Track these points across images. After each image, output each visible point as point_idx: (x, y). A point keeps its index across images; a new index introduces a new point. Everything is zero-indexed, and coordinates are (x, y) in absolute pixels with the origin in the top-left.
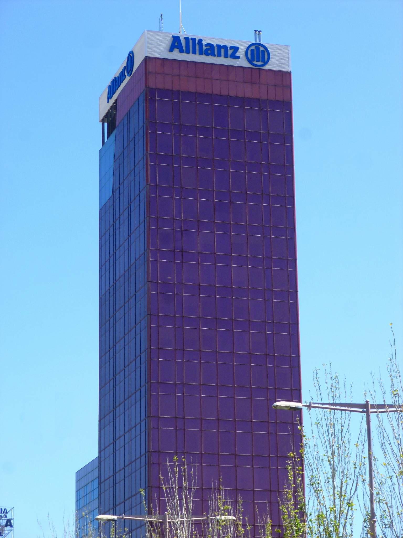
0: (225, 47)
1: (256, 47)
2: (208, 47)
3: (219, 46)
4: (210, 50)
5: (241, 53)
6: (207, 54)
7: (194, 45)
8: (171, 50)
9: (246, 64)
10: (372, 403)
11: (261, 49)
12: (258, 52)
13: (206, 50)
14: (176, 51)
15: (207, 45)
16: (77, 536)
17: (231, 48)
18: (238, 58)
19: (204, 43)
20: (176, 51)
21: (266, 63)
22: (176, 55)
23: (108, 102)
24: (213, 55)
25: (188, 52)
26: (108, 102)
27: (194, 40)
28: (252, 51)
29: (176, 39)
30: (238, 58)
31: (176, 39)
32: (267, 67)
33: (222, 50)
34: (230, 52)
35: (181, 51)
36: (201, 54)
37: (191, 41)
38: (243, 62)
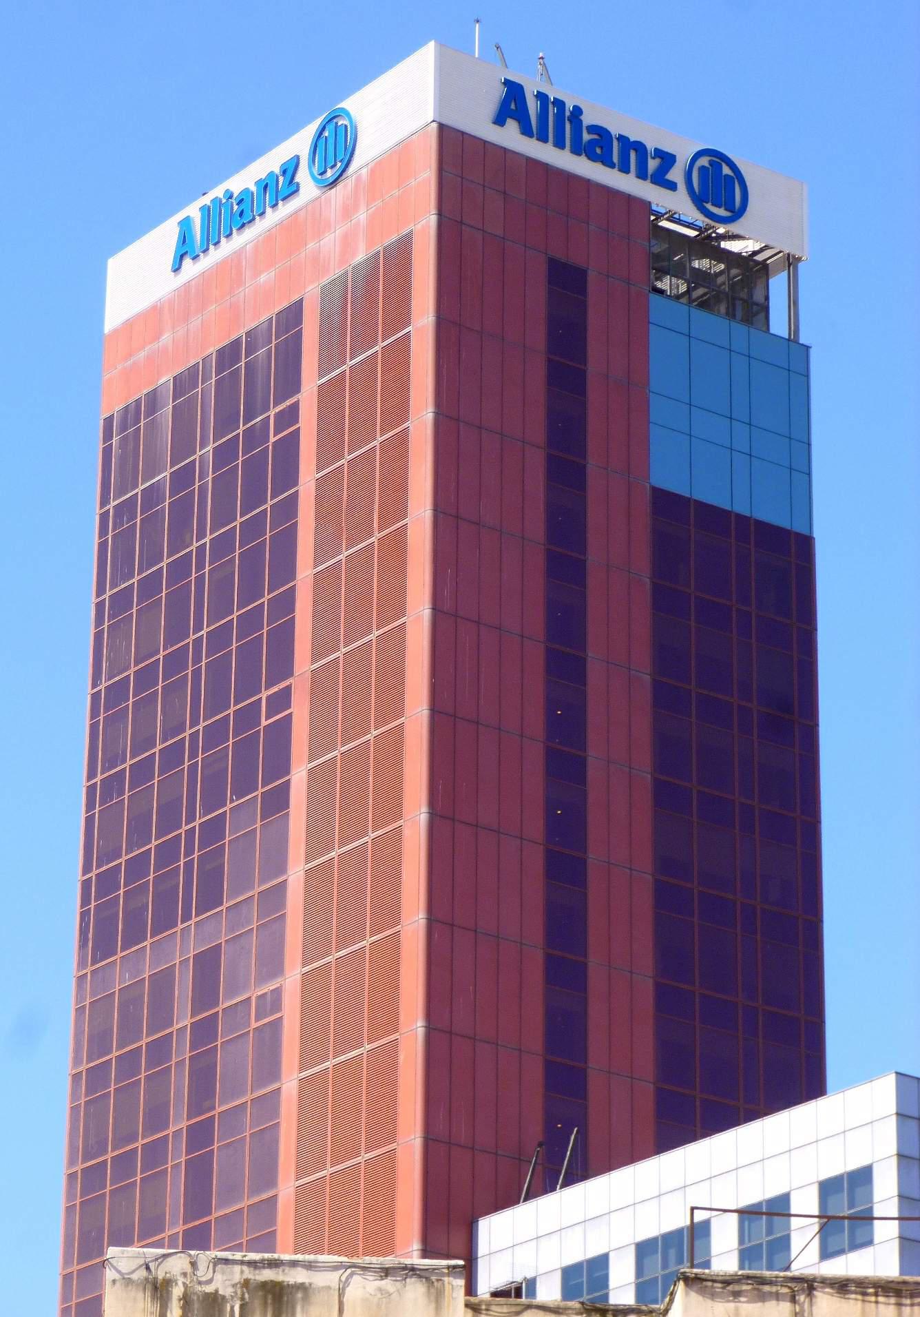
0: (639, 147)
1: (711, 163)
2: (596, 137)
3: (622, 138)
4: (600, 145)
6: (592, 157)
7: (561, 122)
8: (500, 120)
10: (675, 484)
11: (726, 170)
13: (590, 141)
14: (512, 126)
15: (593, 129)
16: (65, 1311)
17: (659, 153)
19: (587, 119)
20: (512, 126)
22: (510, 137)
23: (177, 269)
24: (607, 161)
25: (543, 138)
26: (177, 269)
27: (559, 104)
28: (702, 168)
29: (514, 92)
30: (672, 186)
31: (514, 92)
33: (631, 154)
34: (652, 164)
35: (526, 131)
36: (576, 150)
37: (552, 110)
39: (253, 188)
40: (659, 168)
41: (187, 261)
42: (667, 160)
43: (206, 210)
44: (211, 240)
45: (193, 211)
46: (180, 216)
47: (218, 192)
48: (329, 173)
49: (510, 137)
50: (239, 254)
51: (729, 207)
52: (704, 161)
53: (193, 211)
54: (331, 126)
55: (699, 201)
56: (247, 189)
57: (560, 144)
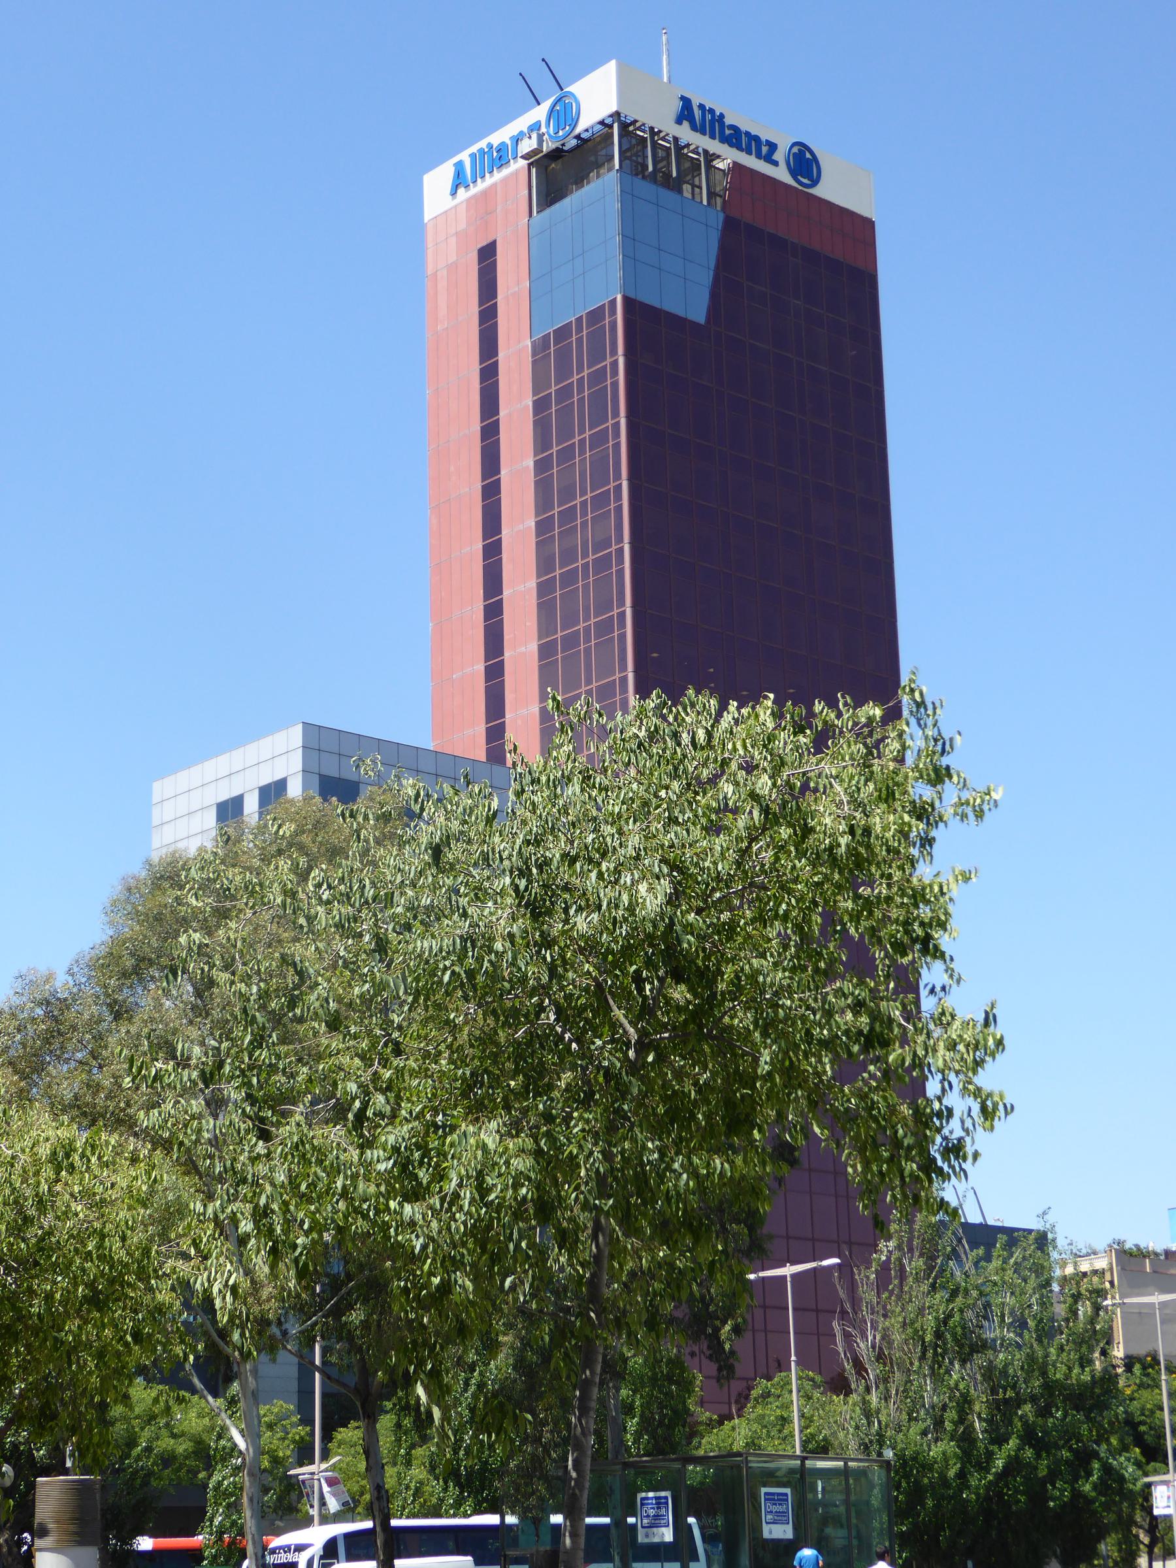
0: (757, 139)
2: (424, 1417)
3: (747, 134)
5: (779, 156)
8: (679, 121)
9: (787, 179)
11: (808, 155)
12: (805, 163)
14: (686, 124)
15: (732, 127)
17: (768, 143)
18: (776, 164)
19: (728, 121)
21: (815, 182)
22: (685, 134)
23: (454, 193)
26: (454, 193)
27: (712, 111)
29: (686, 102)
30: (776, 164)
31: (686, 102)
32: (813, 191)
34: (765, 149)
35: (694, 128)
38: (781, 174)
39: (509, 142)
40: (768, 151)
41: (461, 191)
42: (773, 147)
43: (473, 156)
44: (479, 173)
45: (464, 156)
46: (456, 159)
47: (483, 144)
48: (561, 133)
49: (685, 134)
50: (494, 185)
51: (810, 178)
52: (795, 150)
53: (464, 156)
54: (561, 103)
55: (794, 173)
56: (503, 143)
57: (713, 137)
